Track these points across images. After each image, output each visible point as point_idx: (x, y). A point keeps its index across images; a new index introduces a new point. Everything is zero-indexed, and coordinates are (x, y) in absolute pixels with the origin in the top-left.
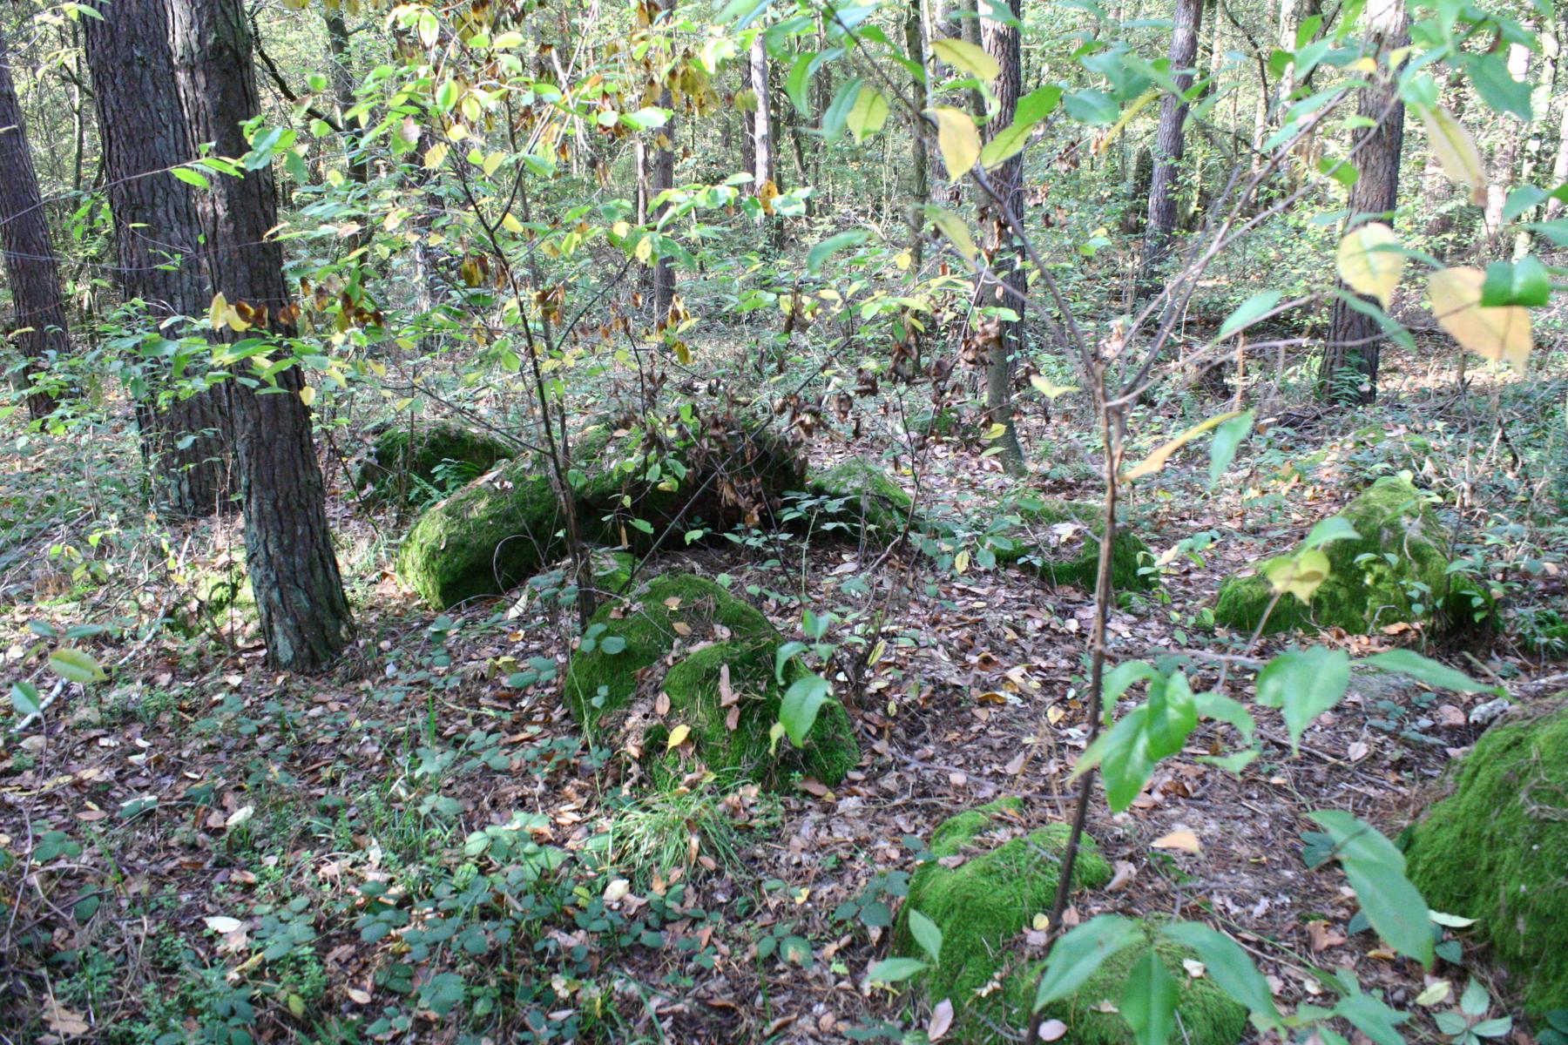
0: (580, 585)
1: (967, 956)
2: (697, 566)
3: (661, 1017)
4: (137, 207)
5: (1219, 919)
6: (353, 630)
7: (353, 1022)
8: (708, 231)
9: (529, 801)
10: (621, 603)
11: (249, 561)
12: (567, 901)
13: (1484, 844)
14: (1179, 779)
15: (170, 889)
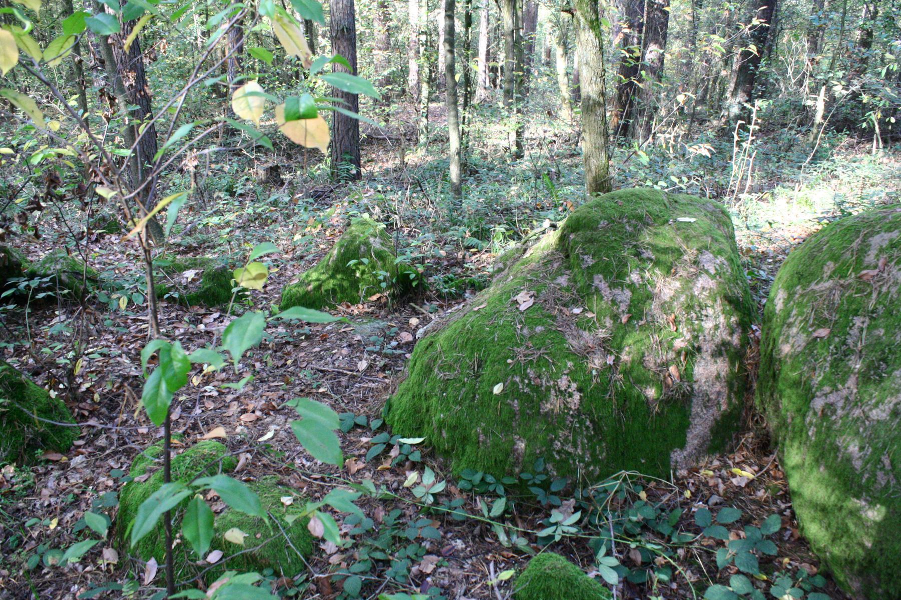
5: (300, 471)
13: (423, 398)
14: (269, 401)
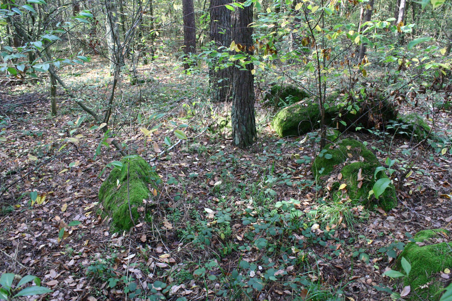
0: (322, 137)
1: (419, 274)
2: (358, 138)
3: (320, 266)
4: (217, 16)
6: (256, 139)
7: (236, 244)
8: (380, 36)
9: (296, 196)
10: (333, 145)
11: (232, 115)
12: (301, 226)
15: (197, 198)
